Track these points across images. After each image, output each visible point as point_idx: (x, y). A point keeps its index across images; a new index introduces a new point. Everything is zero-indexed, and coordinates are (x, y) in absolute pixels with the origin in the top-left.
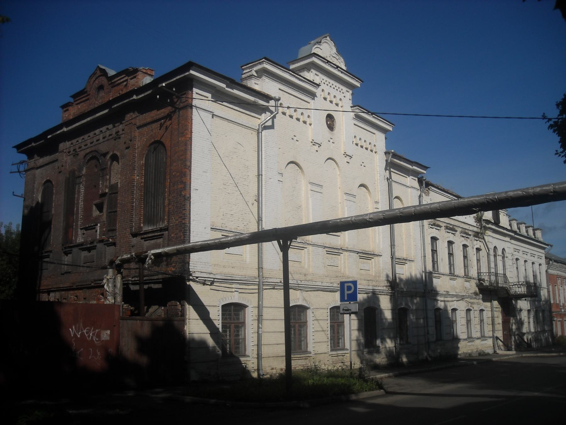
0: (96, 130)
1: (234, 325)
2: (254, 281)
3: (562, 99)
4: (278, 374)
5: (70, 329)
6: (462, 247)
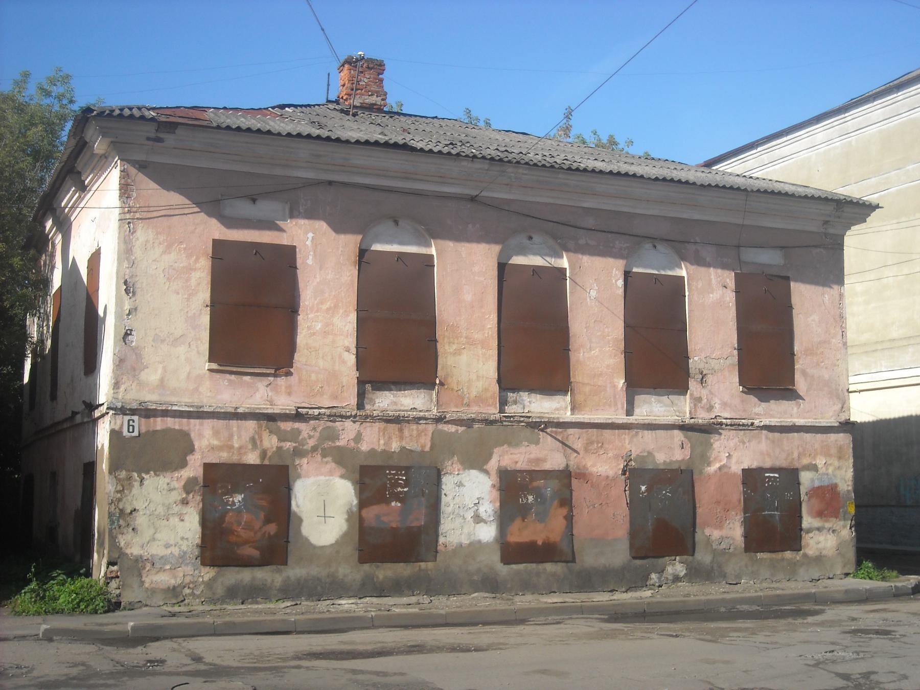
2: (766, 149)
4: (740, 386)
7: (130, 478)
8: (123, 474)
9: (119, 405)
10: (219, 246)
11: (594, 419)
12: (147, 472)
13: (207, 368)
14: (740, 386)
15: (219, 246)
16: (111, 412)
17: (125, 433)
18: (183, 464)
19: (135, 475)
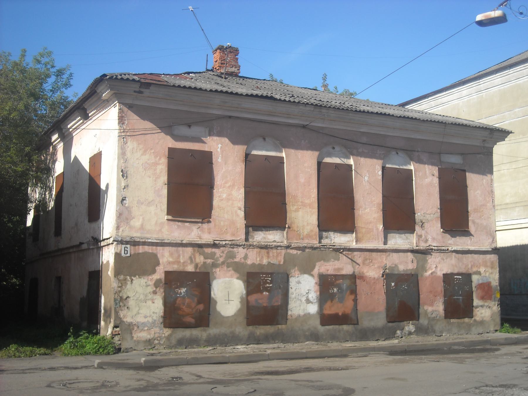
0: (99, 300)
3: (486, 175)
5: (265, 276)
7: (125, 280)
8: (122, 277)
9: (120, 239)
10: (172, 152)
11: (368, 247)
12: (135, 276)
13: (166, 219)
14: (441, 228)
15: (172, 152)
16: (115, 243)
17: (123, 254)
18: (154, 272)
19: (128, 277)
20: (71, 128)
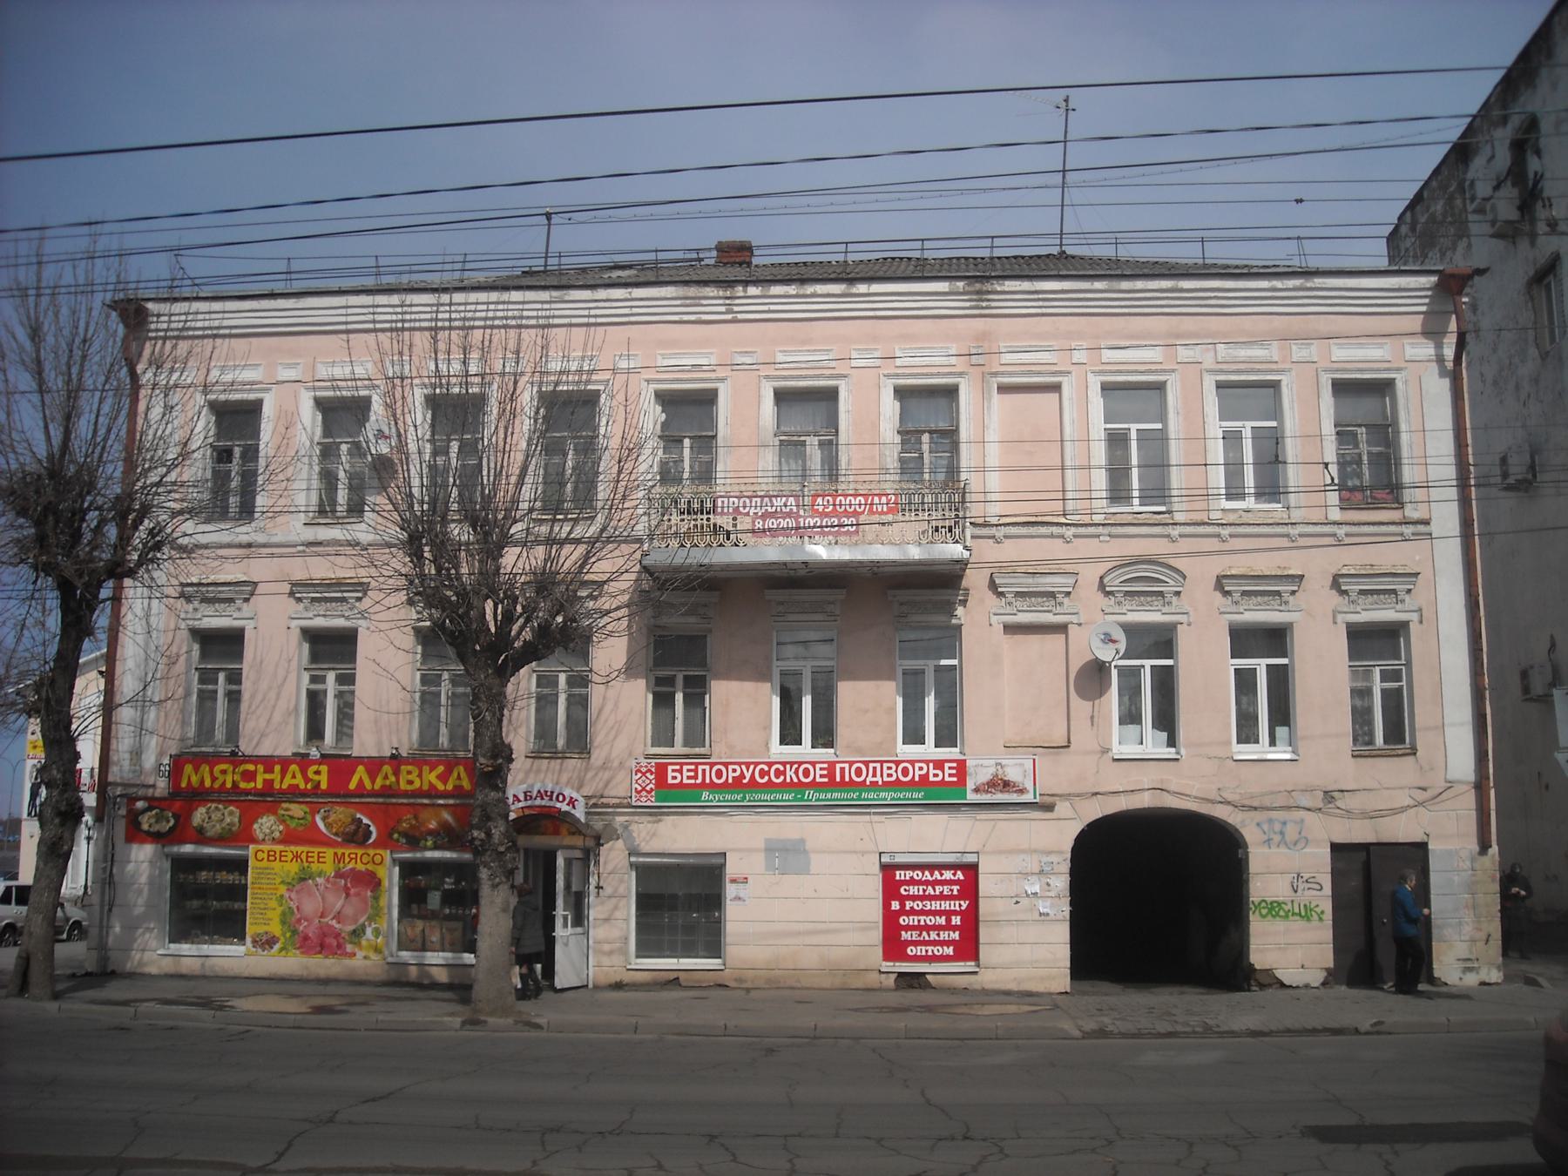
1: (714, 947)
2: (1374, 524)
6: (1432, 524)
15: (242, 663)
20: (1426, 297)
